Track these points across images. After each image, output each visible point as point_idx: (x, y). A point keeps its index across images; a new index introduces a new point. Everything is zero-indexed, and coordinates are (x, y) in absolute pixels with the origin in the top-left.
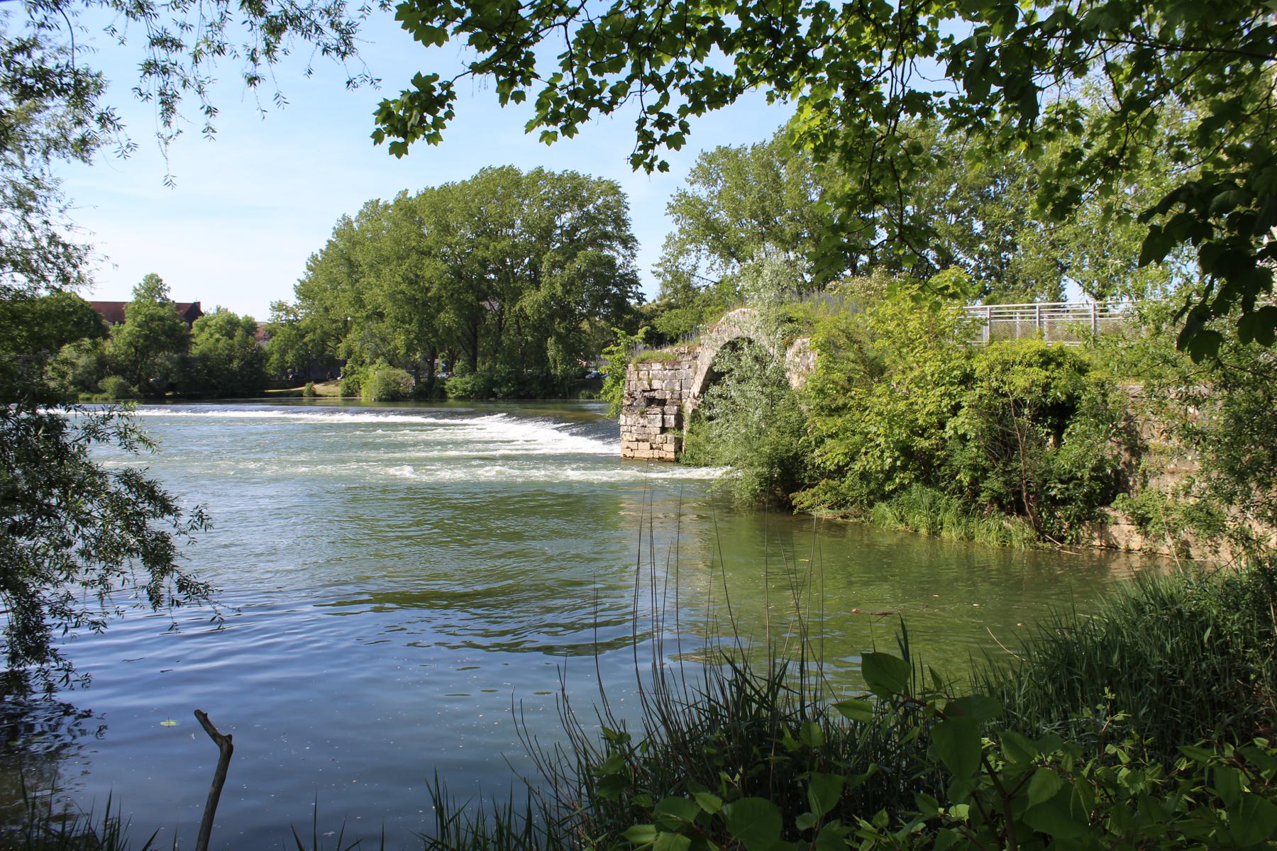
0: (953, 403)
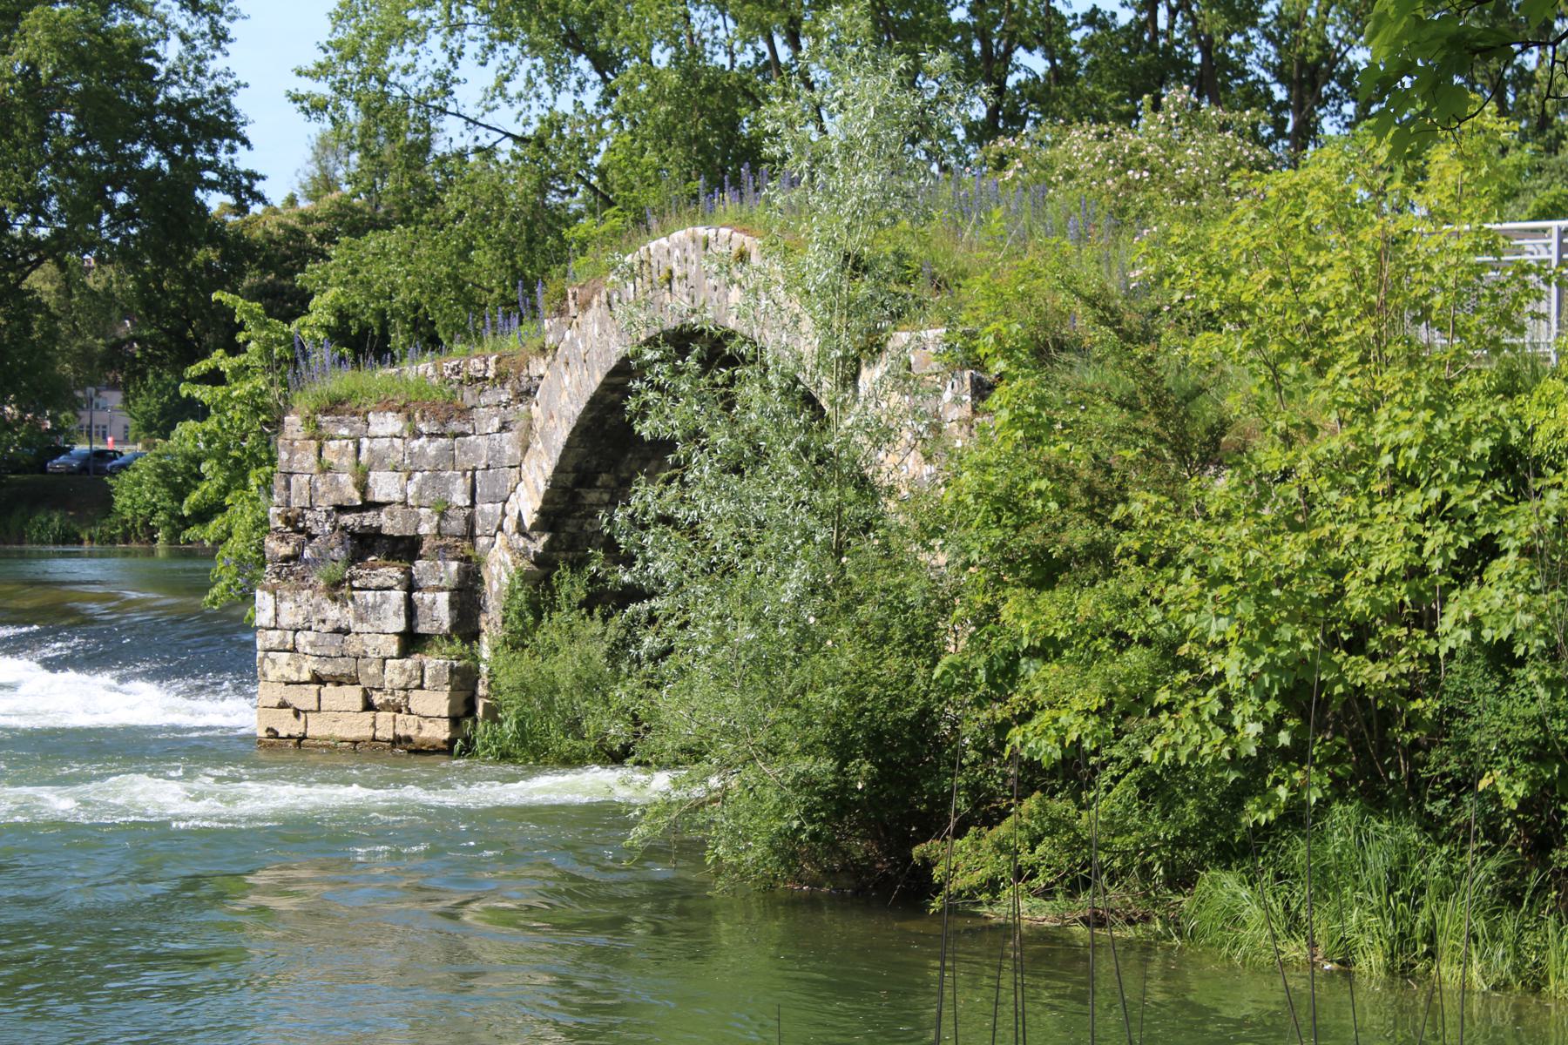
0: (1465, 542)
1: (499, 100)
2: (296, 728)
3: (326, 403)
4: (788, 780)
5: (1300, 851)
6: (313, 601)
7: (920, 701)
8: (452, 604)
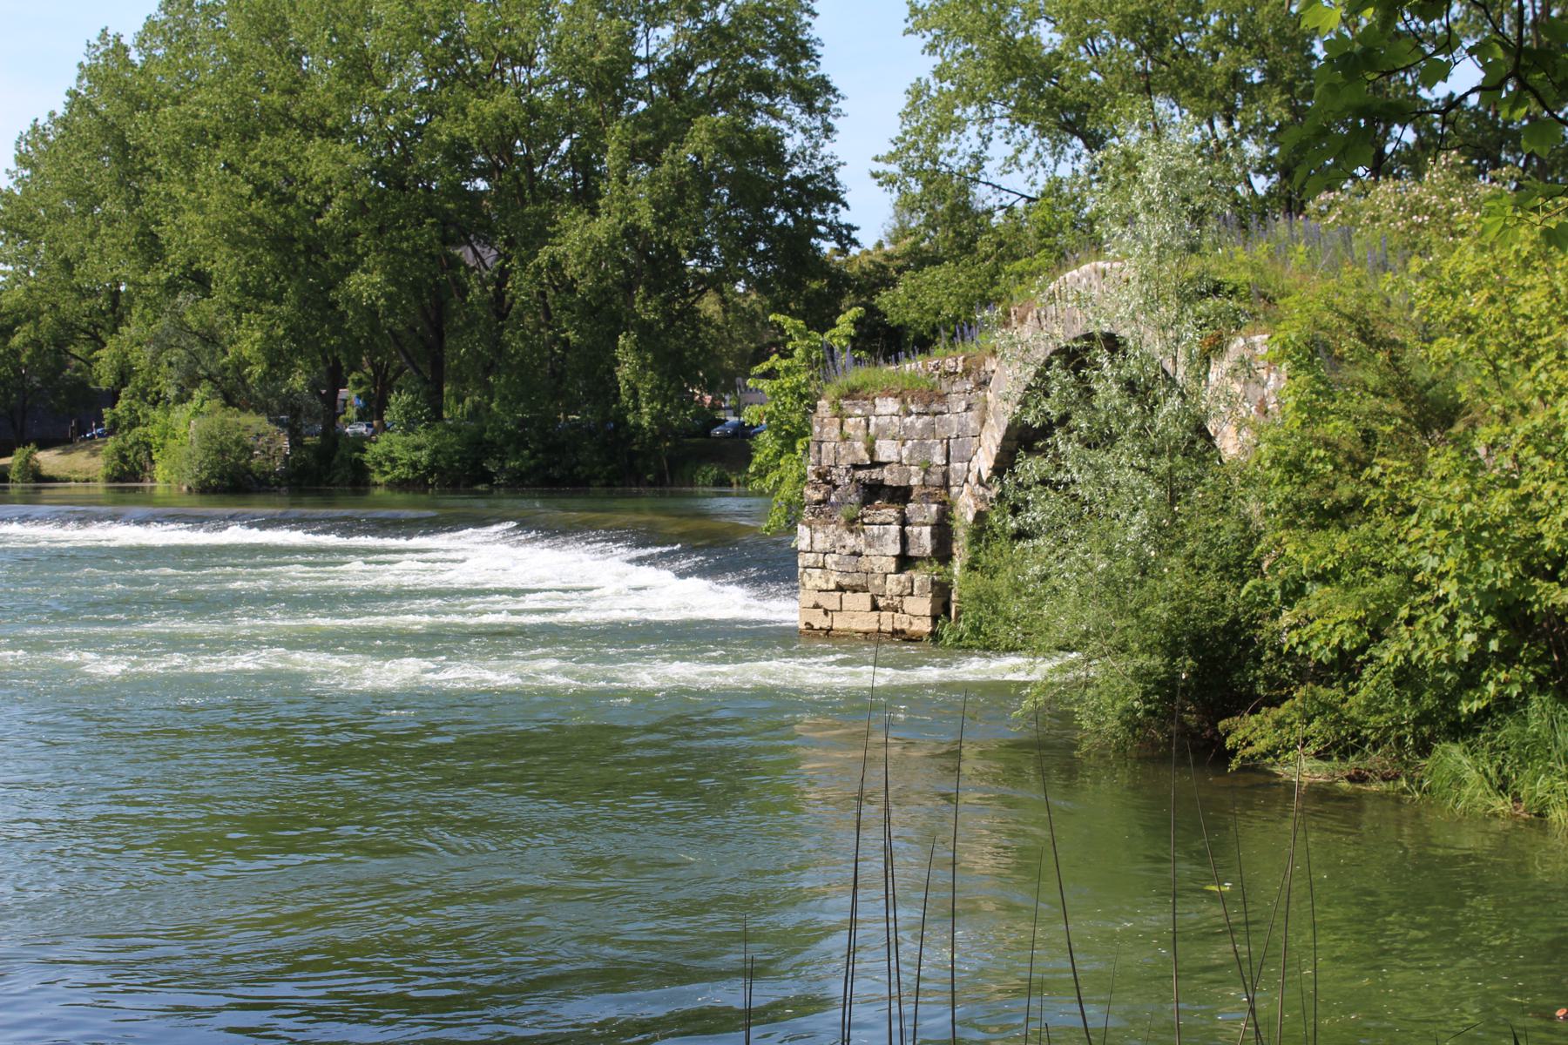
4: (1129, 672)
5: (1510, 729)
7: (1230, 614)
8: (933, 535)
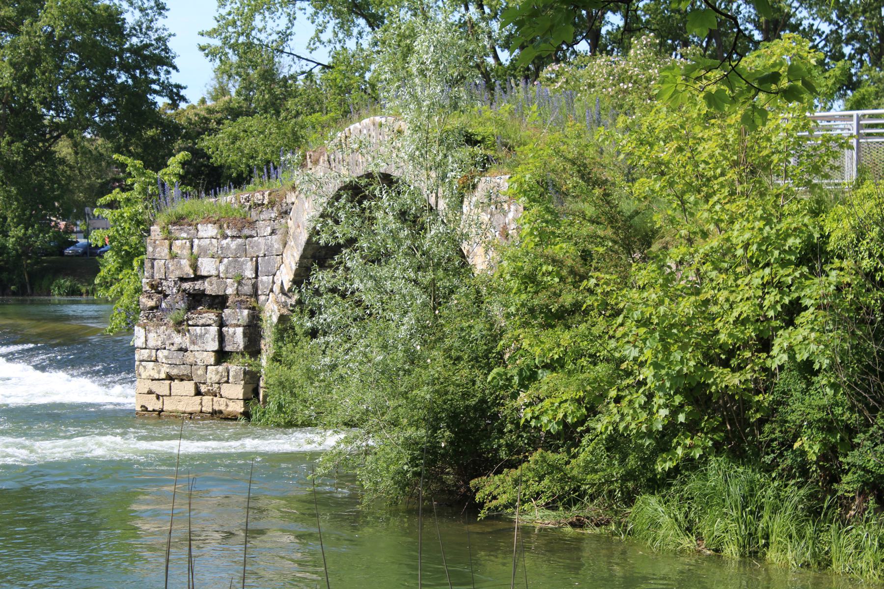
1: (318, 44)
2: (158, 406)
3: (174, 219)
4: (400, 442)
6: (166, 333)
8: (245, 334)
